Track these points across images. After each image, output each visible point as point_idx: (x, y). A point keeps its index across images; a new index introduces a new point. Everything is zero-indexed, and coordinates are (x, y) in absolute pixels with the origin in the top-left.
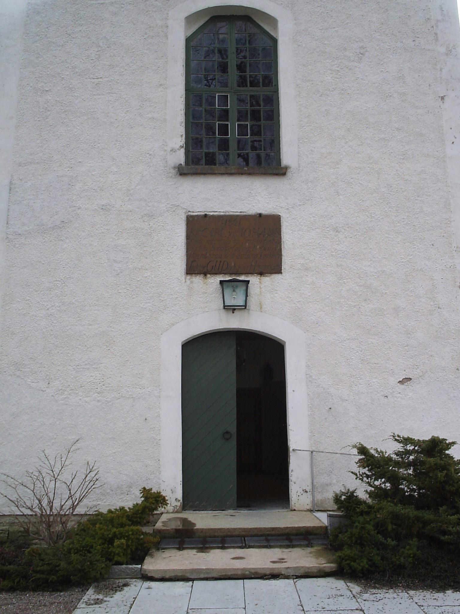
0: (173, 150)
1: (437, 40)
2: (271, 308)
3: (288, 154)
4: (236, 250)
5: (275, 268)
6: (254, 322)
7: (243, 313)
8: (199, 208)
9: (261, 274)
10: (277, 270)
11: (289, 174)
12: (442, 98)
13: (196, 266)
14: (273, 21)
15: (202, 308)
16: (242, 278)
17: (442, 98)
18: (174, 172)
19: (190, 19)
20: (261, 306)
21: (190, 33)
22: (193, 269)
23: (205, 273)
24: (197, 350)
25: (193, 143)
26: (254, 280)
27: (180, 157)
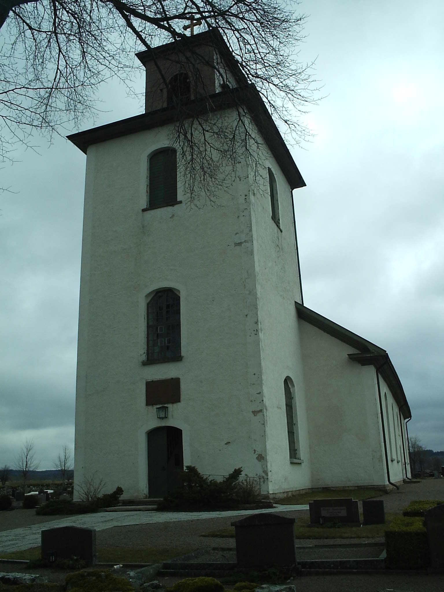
0: (141, 355)
1: (245, 288)
2: (178, 416)
3: (184, 352)
4: (164, 394)
5: (178, 400)
6: (171, 423)
7: (165, 420)
8: (150, 378)
9: (173, 403)
10: (180, 402)
11: (183, 360)
12: (247, 315)
13: (149, 402)
14: (179, 291)
15: (151, 420)
16: (166, 405)
17: (247, 315)
18: (141, 364)
19: (147, 296)
20: (173, 416)
21: (148, 302)
22: (148, 404)
23: (153, 405)
24: (153, 435)
25: (149, 353)
26: (170, 406)
27: (144, 358)
